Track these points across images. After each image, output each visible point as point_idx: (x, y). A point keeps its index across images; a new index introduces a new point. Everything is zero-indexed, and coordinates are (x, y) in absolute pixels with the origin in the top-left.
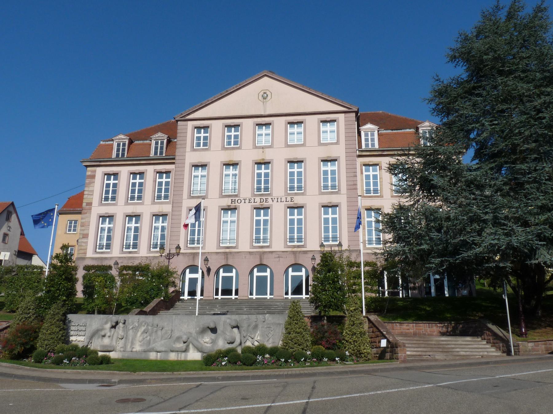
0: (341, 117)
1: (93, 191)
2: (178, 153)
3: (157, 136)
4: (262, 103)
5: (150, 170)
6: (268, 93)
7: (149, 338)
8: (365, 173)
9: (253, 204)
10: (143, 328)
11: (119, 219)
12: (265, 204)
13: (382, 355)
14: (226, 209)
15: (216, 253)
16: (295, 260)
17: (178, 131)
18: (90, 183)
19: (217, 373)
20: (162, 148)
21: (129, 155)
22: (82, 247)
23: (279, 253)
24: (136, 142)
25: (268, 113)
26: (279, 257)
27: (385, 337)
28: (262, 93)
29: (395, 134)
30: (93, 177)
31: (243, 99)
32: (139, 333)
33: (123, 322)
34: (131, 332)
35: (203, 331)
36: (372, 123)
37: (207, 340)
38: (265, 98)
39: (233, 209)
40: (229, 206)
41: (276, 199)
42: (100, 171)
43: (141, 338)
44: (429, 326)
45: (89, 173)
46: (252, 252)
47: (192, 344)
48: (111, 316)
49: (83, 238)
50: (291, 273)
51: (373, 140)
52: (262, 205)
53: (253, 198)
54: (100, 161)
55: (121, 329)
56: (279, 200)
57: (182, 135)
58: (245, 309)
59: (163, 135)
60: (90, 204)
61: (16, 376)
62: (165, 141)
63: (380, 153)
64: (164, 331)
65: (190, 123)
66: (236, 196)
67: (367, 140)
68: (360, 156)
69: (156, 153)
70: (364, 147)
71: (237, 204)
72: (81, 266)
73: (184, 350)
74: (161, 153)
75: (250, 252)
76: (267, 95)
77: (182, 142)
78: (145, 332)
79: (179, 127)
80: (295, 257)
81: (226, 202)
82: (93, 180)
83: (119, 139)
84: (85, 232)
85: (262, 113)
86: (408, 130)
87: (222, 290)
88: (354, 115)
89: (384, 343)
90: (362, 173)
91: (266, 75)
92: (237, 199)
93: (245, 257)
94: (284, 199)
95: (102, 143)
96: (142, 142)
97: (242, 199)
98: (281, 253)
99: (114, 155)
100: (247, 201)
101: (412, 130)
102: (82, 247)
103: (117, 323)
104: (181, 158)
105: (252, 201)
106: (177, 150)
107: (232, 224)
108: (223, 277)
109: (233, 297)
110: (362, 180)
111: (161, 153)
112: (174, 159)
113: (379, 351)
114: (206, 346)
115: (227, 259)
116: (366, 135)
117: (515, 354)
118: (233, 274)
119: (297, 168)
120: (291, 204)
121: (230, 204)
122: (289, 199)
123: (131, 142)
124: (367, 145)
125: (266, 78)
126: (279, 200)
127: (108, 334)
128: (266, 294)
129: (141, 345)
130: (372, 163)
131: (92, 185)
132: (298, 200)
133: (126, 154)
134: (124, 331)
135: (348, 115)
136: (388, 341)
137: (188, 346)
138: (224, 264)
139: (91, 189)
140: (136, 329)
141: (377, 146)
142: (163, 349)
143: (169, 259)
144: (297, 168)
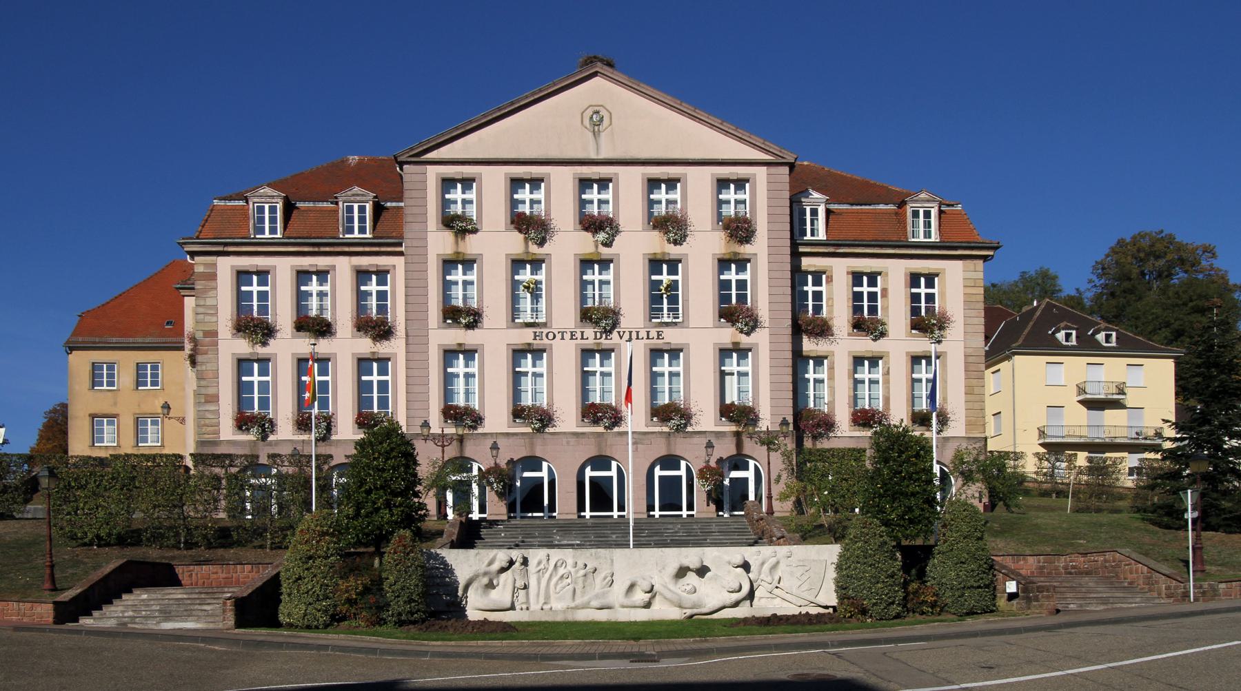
1: (215, 307)
4: (591, 134)
5: (344, 267)
6: (604, 112)
12: (537, 343)
15: (508, 434)
18: (205, 290)
19: (268, 635)
25: (604, 155)
28: (589, 112)
29: (858, 212)
30: (212, 276)
31: (547, 125)
33: (520, 560)
42: (226, 266)
46: (583, 434)
48: (618, 553)
52: (599, 344)
53: (578, 331)
54: (226, 244)
57: (414, 194)
59: (276, 193)
63: (831, 250)
66: (545, 325)
71: (545, 341)
73: (508, 605)
80: (669, 444)
82: (212, 284)
84: (211, 391)
85: (593, 156)
86: (882, 207)
88: (786, 170)
92: (545, 331)
93: (568, 443)
94: (643, 334)
96: (311, 205)
102: (207, 421)
103: (511, 563)
105: (579, 335)
107: (674, 379)
108: (660, 477)
112: (400, 245)
121: (531, 341)
122: (653, 333)
123: (289, 209)
128: (681, 509)
131: (211, 293)
132: (672, 337)
135: (774, 170)
138: (663, 452)
139: (209, 302)
143: (443, 446)
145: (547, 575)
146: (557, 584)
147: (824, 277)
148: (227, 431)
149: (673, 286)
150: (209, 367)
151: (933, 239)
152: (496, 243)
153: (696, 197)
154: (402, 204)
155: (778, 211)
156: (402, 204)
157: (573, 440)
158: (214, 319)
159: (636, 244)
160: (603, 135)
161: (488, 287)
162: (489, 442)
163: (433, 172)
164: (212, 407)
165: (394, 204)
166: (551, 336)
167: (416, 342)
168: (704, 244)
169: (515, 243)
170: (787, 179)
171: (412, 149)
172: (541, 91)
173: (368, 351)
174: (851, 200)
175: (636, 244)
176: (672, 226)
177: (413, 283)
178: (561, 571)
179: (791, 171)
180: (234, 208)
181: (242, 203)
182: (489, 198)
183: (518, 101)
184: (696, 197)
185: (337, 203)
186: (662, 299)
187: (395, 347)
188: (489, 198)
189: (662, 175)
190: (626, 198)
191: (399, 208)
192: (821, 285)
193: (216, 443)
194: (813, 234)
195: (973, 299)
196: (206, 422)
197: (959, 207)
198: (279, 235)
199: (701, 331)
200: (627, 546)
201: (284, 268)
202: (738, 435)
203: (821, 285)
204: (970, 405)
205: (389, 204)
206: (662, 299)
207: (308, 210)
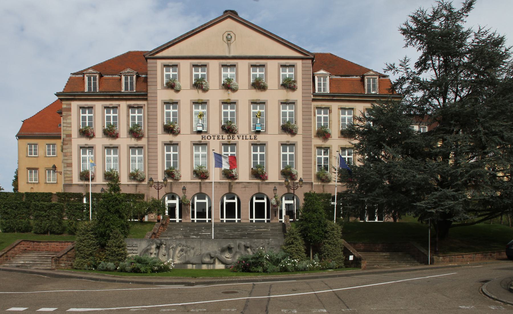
0: (299, 63)
2: (150, 90)
3: (126, 71)
4: (226, 45)
5: (123, 105)
6: (232, 35)
8: (317, 115)
9: (221, 140)
10: (179, 248)
11: (99, 149)
12: (232, 141)
14: (197, 144)
15: (191, 182)
16: (259, 190)
17: (149, 69)
20: (132, 83)
22: (68, 175)
23: (244, 184)
24: (105, 76)
25: (232, 54)
26: (245, 187)
28: (226, 34)
30: (69, 110)
32: (177, 252)
34: (171, 251)
35: (223, 251)
37: (227, 256)
38: (229, 40)
39: (204, 145)
40: (200, 141)
42: (75, 105)
43: (179, 255)
45: (64, 106)
46: (222, 183)
47: (218, 259)
49: (68, 166)
51: (324, 85)
52: (229, 142)
53: (221, 135)
54: (74, 95)
55: (164, 248)
56: (244, 138)
57: (152, 72)
58: (227, 231)
61: (115, 281)
64: (195, 250)
65: (159, 62)
66: (206, 132)
67: (319, 85)
68: (314, 100)
69: (126, 88)
70: (317, 92)
71: (207, 140)
74: (132, 89)
75: (219, 183)
76: (231, 37)
77: (152, 80)
78: (182, 250)
79: (149, 65)
81: (198, 138)
82: (69, 113)
83: (89, 73)
84: (69, 161)
85: (227, 54)
86: (355, 77)
87: (197, 213)
88: (310, 61)
90: (315, 115)
92: (207, 135)
94: (248, 137)
97: (211, 136)
98: (247, 184)
99: (86, 90)
100: (216, 138)
101: (358, 78)
102: (68, 175)
104: (153, 95)
105: (221, 137)
108: (256, 203)
110: (315, 121)
111: (132, 89)
114: (228, 261)
115: (200, 187)
116: (319, 80)
117: (431, 264)
118: (206, 201)
120: (254, 141)
124: (320, 89)
126: (244, 138)
127: (155, 252)
129: (179, 260)
130: (324, 107)
131: (69, 117)
132: (261, 138)
133: (98, 88)
134: (166, 250)
135: (305, 61)
136: (354, 257)
137: (215, 260)
139: (68, 121)
140: (174, 249)
141: (328, 91)
142: (196, 262)
143: (158, 189)
148: (76, 180)
150: (68, 150)
152: (244, 95)
158: (70, 129)
160: (232, 45)
164: (69, 169)
166: (209, 138)
176: (258, 85)
185: (121, 76)
199: (273, 138)
207: (109, 79)
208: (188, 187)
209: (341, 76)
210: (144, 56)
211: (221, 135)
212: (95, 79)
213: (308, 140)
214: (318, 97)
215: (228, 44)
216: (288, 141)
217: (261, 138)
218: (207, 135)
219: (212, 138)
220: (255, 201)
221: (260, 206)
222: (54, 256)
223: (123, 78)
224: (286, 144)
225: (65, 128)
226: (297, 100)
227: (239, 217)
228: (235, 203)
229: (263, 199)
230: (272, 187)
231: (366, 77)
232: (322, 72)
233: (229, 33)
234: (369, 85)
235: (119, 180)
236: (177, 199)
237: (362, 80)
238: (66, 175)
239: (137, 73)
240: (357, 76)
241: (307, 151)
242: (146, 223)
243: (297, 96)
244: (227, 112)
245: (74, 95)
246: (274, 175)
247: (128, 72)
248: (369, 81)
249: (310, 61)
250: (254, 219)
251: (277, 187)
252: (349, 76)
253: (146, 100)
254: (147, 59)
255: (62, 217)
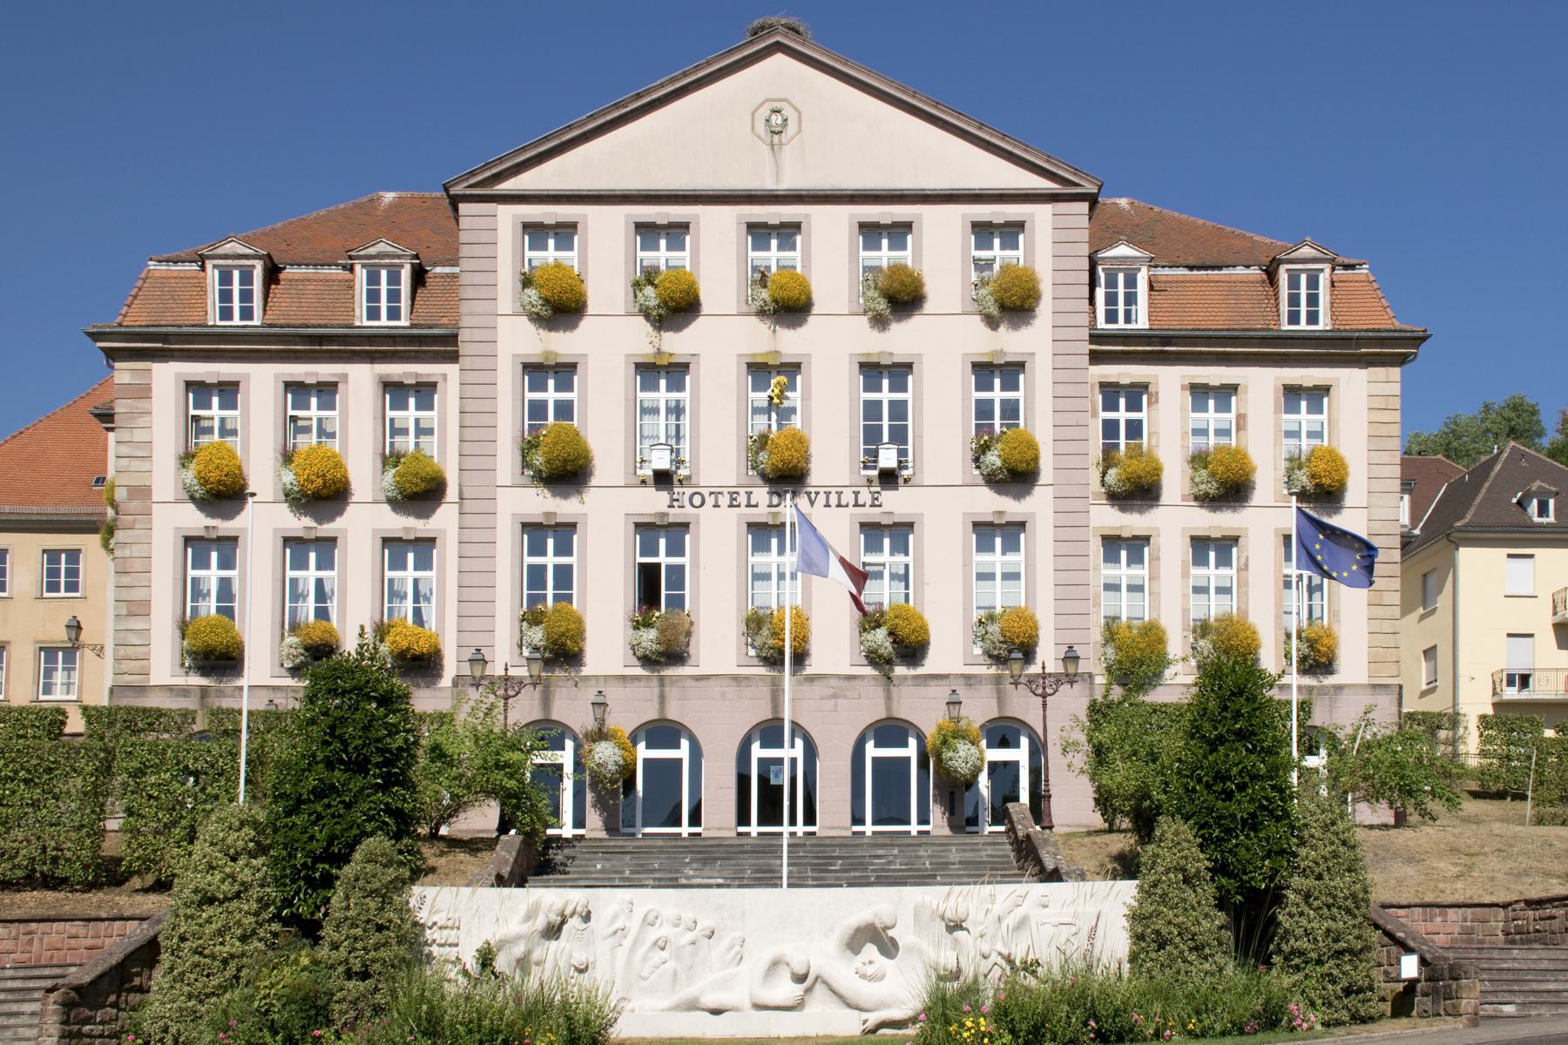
0: (1041, 217)
4: (767, 148)
6: (788, 112)
7: (671, 964)
12: (676, 515)
13: (1404, 1003)
15: (623, 678)
16: (889, 708)
18: (132, 415)
21: (270, 318)
22: (131, 651)
23: (833, 682)
26: (834, 696)
27: (1409, 950)
28: (765, 112)
30: (144, 392)
31: (697, 135)
36: (1130, 242)
40: (665, 515)
41: (822, 497)
42: (167, 377)
44: (1424, 914)
46: (747, 678)
49: (130, 615)
50: (872, 751)
52: (775, 515)
56: (833, 500)
57: (477, 251)
60: (142, 493)
62: (405, 275)
70: (1101, 324)
72: (412, 689)
80: (888, 698)
82: (142, 405)
83: (226, 257)
84: (137, 595)
85: (768, 183)
86: (1240, 270)
88: (1084, 207)
89: (1409, 967)
91: (778, 47)
92: (689, 491)
93: (723, 694)
94: (848, 497)
95: (152, 265)
97: (706, 492)
100: (724, 500)
102: (131, 651)
105: (742, 499)
106: (465, 307)
108: (875, 760)
109: (685, 829)
113: (1400, 987)
115: (662, 699)
118: (683, 752)
119: (891, 390)
125: (779, 59)
126: (833, 500)
128: (908, 823)
131: (141, 422)
132: (896, 503)
136: (1423, 962)
139: (139, 435)
143: (1044, 696)
144: (891, 390)
145: (627, 943)
146: (645, 958)
147: (1145, 398)
148: (165, 667)
149: (899, 410)
150: (136, 551)
151: (1320, 327)
152: (610, 338)
153: (941, 250)
154: (456, 270)
155: (1070, 277)
156: (456, 270)
157: (731, 690)
158: (145, 466)
159: (834, 340)
160: (786, 148)
161: (603, 416)
162: (591, 695)
163: (508, 217)
164: (137, 624)
165: (447, 270)
166: (697, 500)
167: (477, 510)
168: (945, 339)
169: (641, 339)
170: (1084, 221)
171: (472, 174)
172: (698, 68)
173: (650, 350)
174: (1191, 261)
175: (834, 340)
176: (901, 298)
177: (471, 406)
178: (653, 934)
179: (1091, 209)
180: (181, 277)
181: (195, 267)
182: (604, 254)
183: (648, 91)
184: (941, 250)
185: (351, 269)
186: (883, 427)
187: (444, 520)
188: (604, 254)
189: (885, 212)
190: (829, 255)
191: (454, 276)
192: (1140, 409)
193: (142, 689)
194: (1128, 320)
195: (1384, 430)
196: (132, 651)
197: (1364, 271)
198: (256, 322)
199: (944, 496)
200: (777, 885)
201: (262, 382)
202: (998, 680)
203: (1140, 409)
204: (1376, 626)
205: (438, 270)
206: (883, 427)
207: (305, 280)
208: (614, 694)
209: (1191, 268)
210: (446, 189)
211: (742, 491)
212: (247, 278)
213: (1077, 505)
214: (1105, 347)
215: (772, 146)
216: (1001, 513)
217: (896, 503)
218: (689, 491)
219: (710, 501)
220: (872, 751)
221: (892, 773)
222: (60, 981)
223: (361, 274)
224: (991, 524)
225: (124, 462)
226: (920, 355)
227: (810, 818)
228: (680, 761)
229: (905, 745)
230: (941, 693)
231: (1283, 269)
232: (1123, 250)
233: (778, 105)
234: (1294, 300)
235: (1335, 666)
236: (912, 742)
237: (1271, 275)
238: (122, 651)
239: (417, 257)
240: (1248, 267)
241: (1069, 552)
242: (443, 838)
243: (1029, 341)
244: (544, 403)
245: (164, 338)
246: (952, 651)
247: (379, 256)
248: (1294, 283)
249: (1084, 207)
250: (869, 828)
251: (963, 693)
252: (1220, 268)
253: (453, 357)
254: (455, 201)
255: (101, 815)
